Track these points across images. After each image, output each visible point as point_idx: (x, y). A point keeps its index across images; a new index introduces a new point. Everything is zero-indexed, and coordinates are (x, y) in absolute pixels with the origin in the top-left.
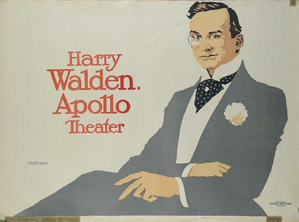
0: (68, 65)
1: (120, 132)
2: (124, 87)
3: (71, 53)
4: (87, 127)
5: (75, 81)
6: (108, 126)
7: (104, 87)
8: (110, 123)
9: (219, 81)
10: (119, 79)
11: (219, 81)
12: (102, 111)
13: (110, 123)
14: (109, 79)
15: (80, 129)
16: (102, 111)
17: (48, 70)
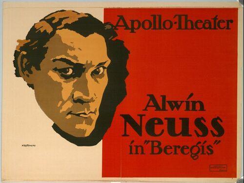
0: (145, 115)
1: (228, 28)
2: (190, 134)
3: (142, 153)
4: (197, 22)
5: (207, 23)
6: (217, 21)
7: (195, 28)
8: (219, 18)
9: (98, 149)
10: (173, 147)
11: (98, 149)
12: (152, 27)
13: (219, 18)
14: (81, 115)
15: (189, 26)
16: (152, 27)
17: (147, 95)
